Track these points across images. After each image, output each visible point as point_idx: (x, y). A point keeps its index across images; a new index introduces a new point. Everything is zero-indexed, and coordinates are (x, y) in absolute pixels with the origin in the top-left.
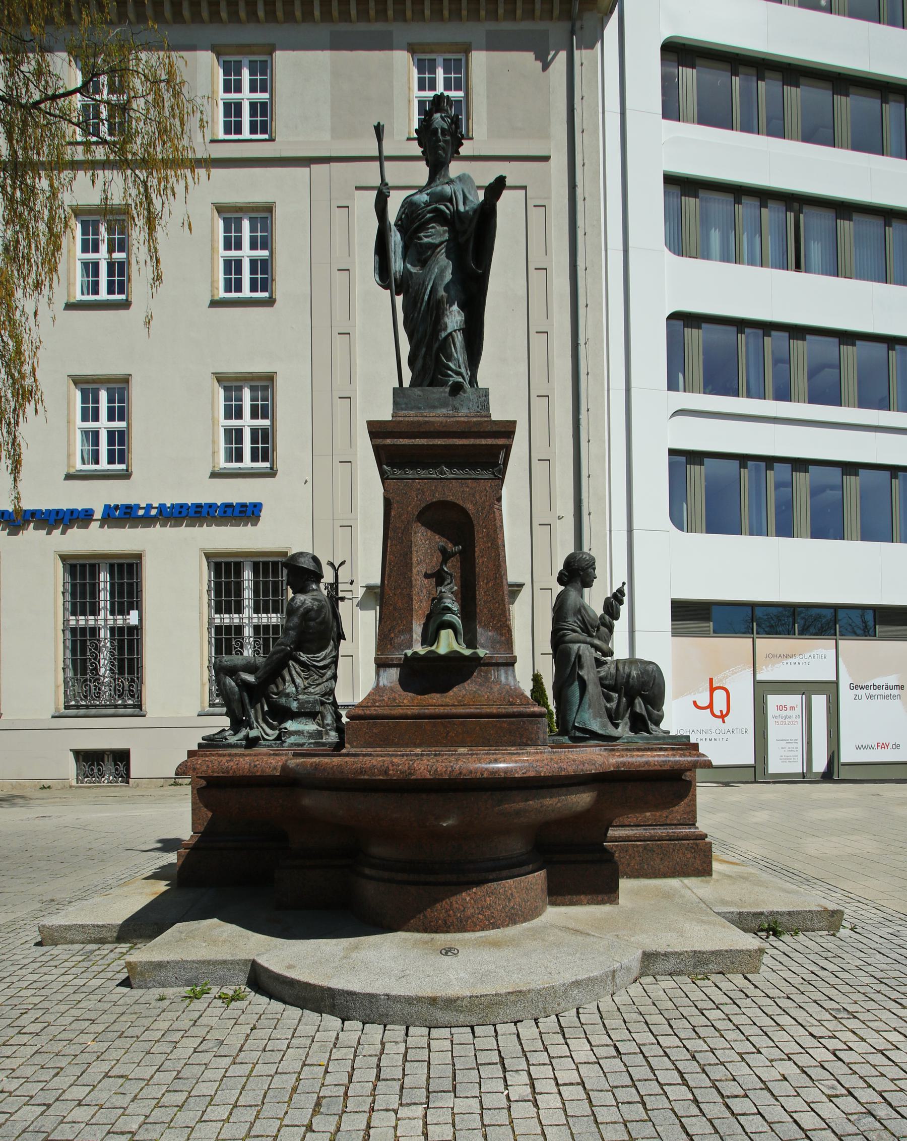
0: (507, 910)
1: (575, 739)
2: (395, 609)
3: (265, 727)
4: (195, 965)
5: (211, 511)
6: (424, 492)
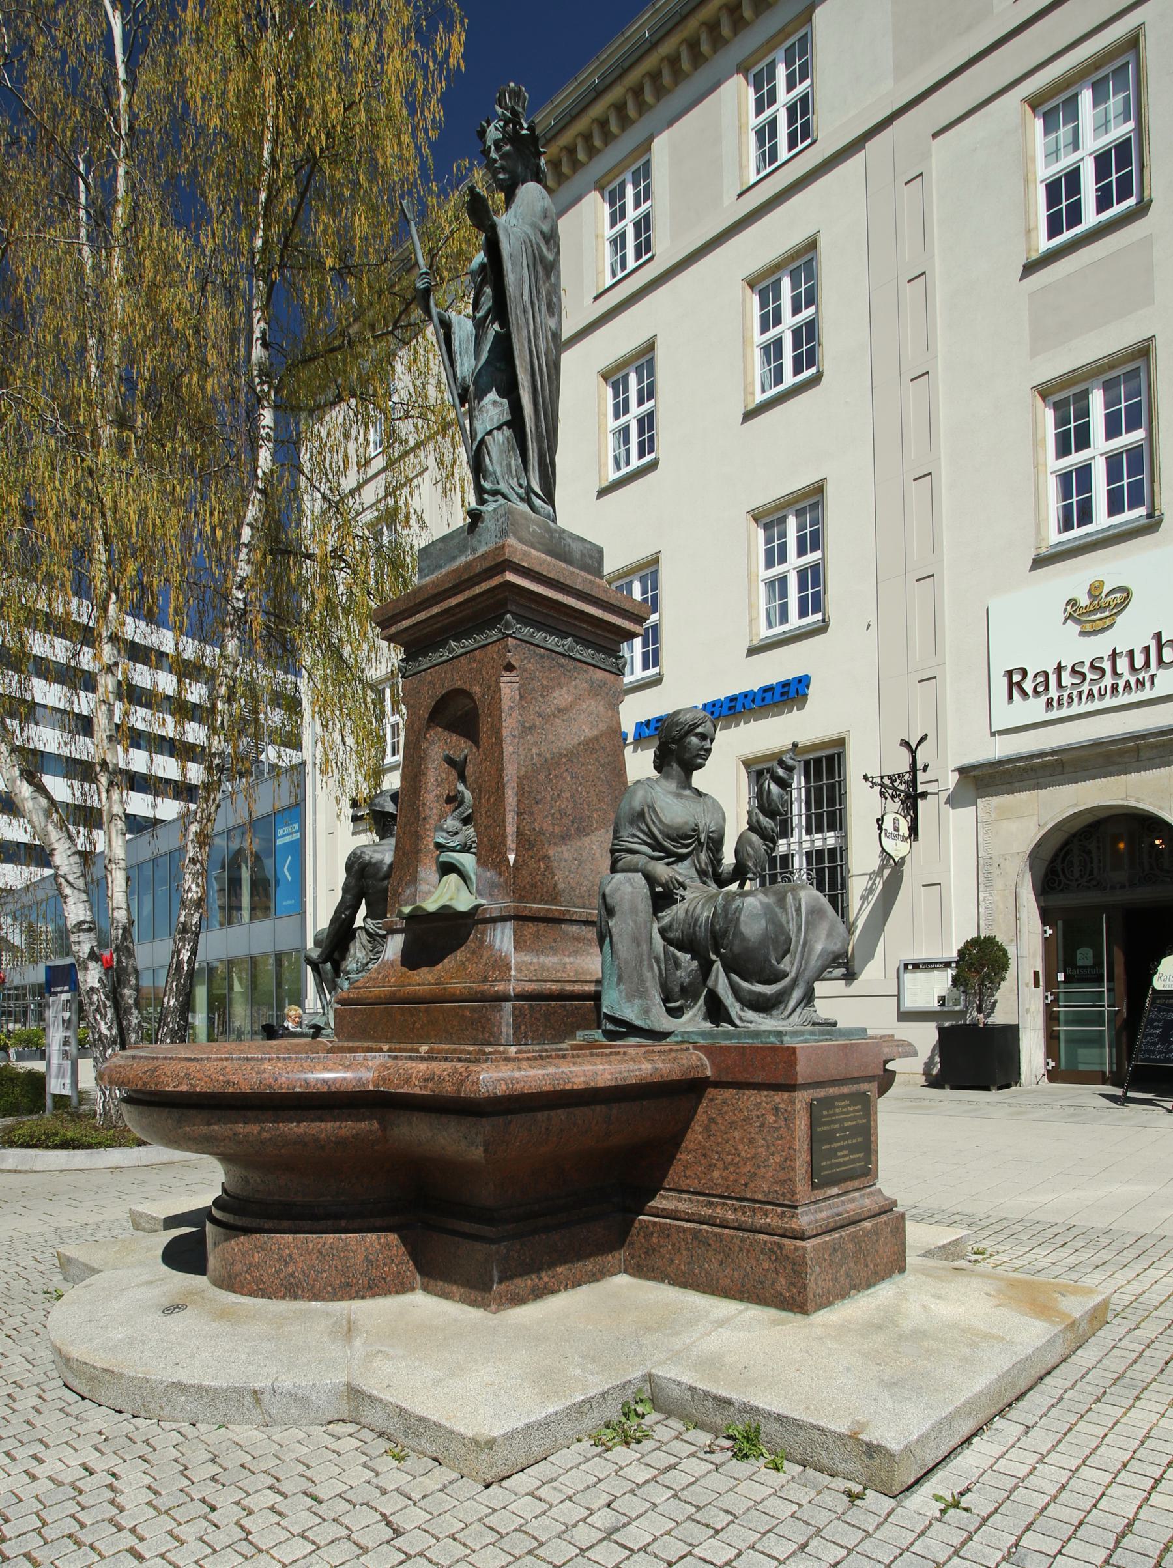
0: (282, 1276)
1: (611, 1035)
5: (748, 702)
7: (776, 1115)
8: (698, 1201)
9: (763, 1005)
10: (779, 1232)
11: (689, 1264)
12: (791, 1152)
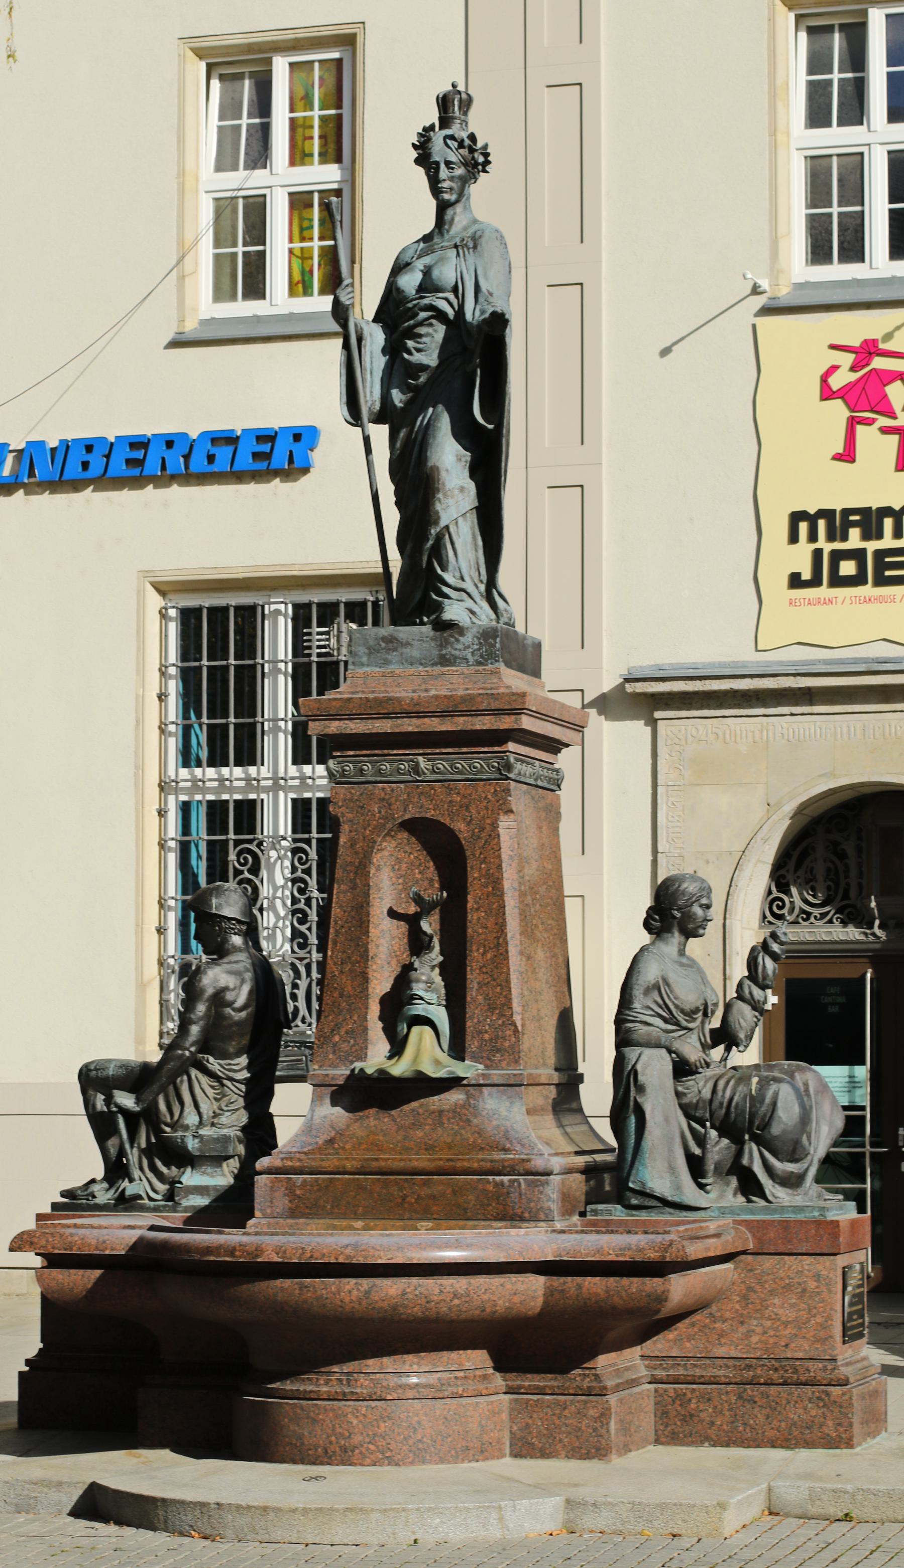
0: (411, 1442)
2: (341, 995)
4: (27, 1486)
6: (390, 805)
7: (818, 1281)
8: (735, 1366)
9: (792, 1182)
10: (825, 1382)
11: (733, 1422)
12: (832, 1312)
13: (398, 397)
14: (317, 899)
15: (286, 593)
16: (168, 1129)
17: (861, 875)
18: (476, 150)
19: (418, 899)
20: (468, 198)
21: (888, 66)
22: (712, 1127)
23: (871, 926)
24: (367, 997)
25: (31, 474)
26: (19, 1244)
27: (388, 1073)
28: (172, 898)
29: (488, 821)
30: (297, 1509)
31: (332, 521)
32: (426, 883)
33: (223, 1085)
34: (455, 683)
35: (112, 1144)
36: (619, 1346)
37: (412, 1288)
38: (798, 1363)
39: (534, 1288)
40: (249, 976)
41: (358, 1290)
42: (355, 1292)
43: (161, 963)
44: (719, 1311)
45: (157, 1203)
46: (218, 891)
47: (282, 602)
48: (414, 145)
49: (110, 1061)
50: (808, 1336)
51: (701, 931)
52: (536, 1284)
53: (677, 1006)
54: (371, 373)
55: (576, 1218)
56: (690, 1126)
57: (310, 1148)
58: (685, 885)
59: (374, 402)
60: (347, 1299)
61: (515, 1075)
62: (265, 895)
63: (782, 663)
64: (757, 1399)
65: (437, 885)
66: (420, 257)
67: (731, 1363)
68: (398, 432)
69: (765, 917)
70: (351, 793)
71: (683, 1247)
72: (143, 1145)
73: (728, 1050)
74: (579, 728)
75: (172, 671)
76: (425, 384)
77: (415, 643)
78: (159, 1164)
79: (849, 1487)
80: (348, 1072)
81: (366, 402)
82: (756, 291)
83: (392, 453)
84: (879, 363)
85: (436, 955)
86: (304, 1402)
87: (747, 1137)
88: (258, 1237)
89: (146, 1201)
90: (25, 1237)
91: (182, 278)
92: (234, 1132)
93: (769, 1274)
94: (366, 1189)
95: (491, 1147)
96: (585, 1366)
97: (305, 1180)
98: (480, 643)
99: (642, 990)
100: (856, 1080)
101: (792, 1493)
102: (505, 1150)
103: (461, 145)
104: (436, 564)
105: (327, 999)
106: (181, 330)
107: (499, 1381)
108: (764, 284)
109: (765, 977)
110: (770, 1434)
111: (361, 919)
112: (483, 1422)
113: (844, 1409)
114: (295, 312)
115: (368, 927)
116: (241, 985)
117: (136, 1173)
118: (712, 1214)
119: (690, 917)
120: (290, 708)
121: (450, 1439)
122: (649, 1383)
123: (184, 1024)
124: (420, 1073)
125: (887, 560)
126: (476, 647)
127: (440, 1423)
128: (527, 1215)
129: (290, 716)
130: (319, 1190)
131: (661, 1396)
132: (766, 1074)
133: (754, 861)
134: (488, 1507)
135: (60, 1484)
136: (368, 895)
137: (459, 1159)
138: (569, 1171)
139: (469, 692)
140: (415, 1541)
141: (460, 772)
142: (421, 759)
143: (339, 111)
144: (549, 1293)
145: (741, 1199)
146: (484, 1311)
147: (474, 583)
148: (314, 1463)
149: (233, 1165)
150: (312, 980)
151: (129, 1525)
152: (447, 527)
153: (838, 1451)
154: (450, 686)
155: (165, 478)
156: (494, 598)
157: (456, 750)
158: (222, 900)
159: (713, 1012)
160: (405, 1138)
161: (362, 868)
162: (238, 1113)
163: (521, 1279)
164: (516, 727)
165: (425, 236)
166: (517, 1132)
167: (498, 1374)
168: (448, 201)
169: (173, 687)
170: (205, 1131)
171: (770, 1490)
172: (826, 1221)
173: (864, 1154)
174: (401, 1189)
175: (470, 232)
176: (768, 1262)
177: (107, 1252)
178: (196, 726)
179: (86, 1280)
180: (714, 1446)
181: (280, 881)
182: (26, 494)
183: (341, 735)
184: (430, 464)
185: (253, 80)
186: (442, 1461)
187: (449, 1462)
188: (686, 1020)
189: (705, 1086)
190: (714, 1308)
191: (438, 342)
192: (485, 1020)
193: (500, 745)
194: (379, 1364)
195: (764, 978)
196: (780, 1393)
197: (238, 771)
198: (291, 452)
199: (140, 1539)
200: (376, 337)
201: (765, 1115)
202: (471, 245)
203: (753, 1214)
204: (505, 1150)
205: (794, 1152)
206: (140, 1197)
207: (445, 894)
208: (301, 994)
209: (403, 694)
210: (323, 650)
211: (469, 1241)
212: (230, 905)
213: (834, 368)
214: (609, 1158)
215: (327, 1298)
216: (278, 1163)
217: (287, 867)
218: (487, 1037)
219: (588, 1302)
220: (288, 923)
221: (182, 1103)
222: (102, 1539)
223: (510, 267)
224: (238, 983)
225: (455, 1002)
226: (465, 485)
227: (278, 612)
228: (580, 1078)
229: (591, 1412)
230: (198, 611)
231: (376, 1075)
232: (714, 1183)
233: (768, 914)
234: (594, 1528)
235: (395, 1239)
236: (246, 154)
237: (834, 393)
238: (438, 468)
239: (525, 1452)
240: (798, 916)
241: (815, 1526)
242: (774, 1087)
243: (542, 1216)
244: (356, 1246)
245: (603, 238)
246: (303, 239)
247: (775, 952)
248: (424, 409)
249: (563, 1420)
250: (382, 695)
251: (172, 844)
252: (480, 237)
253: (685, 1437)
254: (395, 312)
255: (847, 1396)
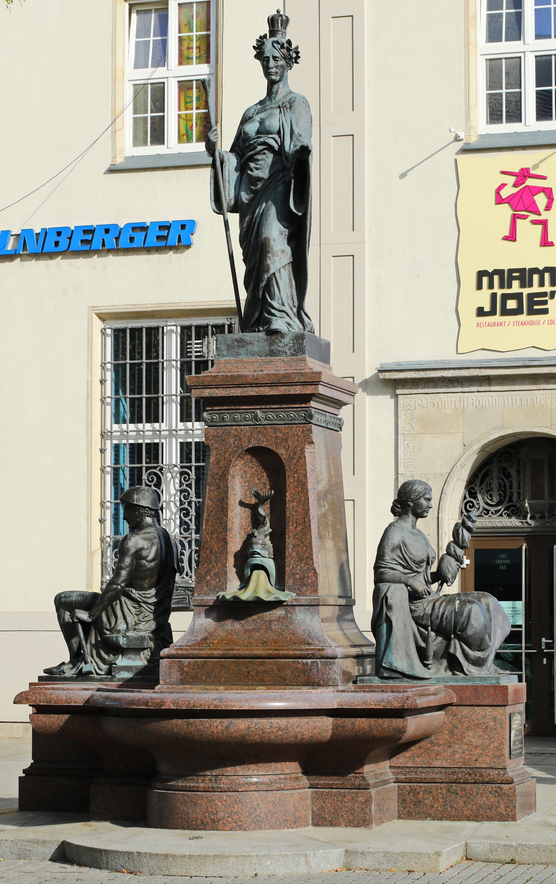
0: (253, 817)
2: (211, 552)
3: (100, 663)
4: (24, 843)
6: (240, 439)
7: (495, 721)
8: (446, 772)
9: (479, 663)
10: (499, 782)
11: (444, 806)
12: (503, 740)
13: (245, 197)
14: (195, 502)
15: (177, 319)
16: (108, 632)
17: (519, 488)
18: (292, 50)
19: (257, 495)
20: (287, 79)
21: (535, 5)
22: (432, 630)
23: (525, 517)
24: (227, 553)
25: (25, 247)
26: (19, 699)
27: (239, 598)
28: (109, 502)
29: (299, 449)
30: (185, 855)
31: (206, 275)
32: (262, 485)
33: (141, 606)
34: (279, 366)
35: (75, 641)
36: (377, 760)
37: (254, 724)
38: (483, 771)
39: (326, 725)
40: (156, 541)
41: (222, 725)
42: (220, 727)
43: (102, 540)
44: (436, 739)
45: (101, 676)
46: (138, 491)
47: (174, 325)
48: (254, 47)
49: (73, 592)
50: (489, 754)
51: (425, 514)
52: (327, 723)
53: (411, 559)
54: (229, 182)
55: (351, 684)
56: (419, 630)
57: (193, 643)
58: (415, 487)
59: (230, 200)
60: (215, 731)
61: (314, 599)
62: (164, 499)
63: (472, 361)
64: (458, 792)
65: (268, 487)
66: (258, 113)
67: (443, 770)
68: (245, 217)
69: (462, 512)
70: (217, 432)
71: (415, 700)
72: (93, 642)
73: (441, 585)
74: (352, 394)
75: (109, 366)
76: (261, 189)
77: (255, 343)
78: (103, 653)
79: (513, 843)
80: (215, 598)
81: (226, 200)
82: (457, 139)
83: (241, 231)
84: (530, 182)
85: (267, 528)
86: (190, 793)
87: (453, 636)
88: (162, 694)
89: (95, 675)
90: (23, 695)
91: (114, 132)
92: (147, 634)
93: (466, 718)
94: (226, 667)
95: (301, 642)
96: (356, 771)
97: (189, 662)
98: (294, 343)
99: (390, 549)
100: (517, 609)
101: (479, 847)
102: (309, 644)
103: (282, 46)
104: (267, 296)
105: (203, 554)
106: (114, 163)
107: (305, 781)
108: (462, 135)
109: (463, 541)
110: (466, 813)
111: (223, 507)
112: (296, 805)
113: (511, 797)
114: (182, 152)
115: (227, 511)
116: (152, 547)
117: (89, 659)
118: (432, 682)
119: (419, 505)
120: (179, 388)
121: (276, 815)
122: (394, 782)
123: (117, 572)
124: (258, 598)
125: (535, 299)
126: (291, 345)
127: (271, 805)
128: (322, 682)
129: (179, 393)
130: (198, 668)
131: (402, 790)
132: (464, 599)
133: (455, 479)
134: (299, 854)
135: (44, 842)
136: (227, 492)
137: (281, 649)
138: (347, 657)
139: (287, 372)
140: (256, 875)
141: (282, 419)
142: (258, 411)
143: (208, 33)
144: (335, 727)
145: (449, 673)
146: (297, 738)
147: (290, 307)
148: (196, 829)
149: (147, 653)
150: (192, 550)
151: (85, 866)
152: (274, 274)
153: (507, 823)
154: (276, 368)
155: (105, 250)
156: (303, 319)
157: (280, 406)
158: (140, 496)
159: (432, 562)
160: (249, 637)
161: (223, 477)
162: (149, 623)
163: (319, 719)
164: (315, 392)
165: (260, 101)
166: (316, 633)
167: (304, 777)
168: (275, 80)
169: (109, 376)
170: (130, 634)
171: (466, 845)
172: (500, 686)
173: (521, 654)
174: (247, 667)
175: (288, 98)
176: (465, 711)
177: (72, 704)
178: (123, 399)
179: (59, 721)
180: (433, 820)
181: (173, 492)
182: (21, 261)
183: (211, 397)
184: (264, 236)
185: (157, 14)
186: (271, 828)
187: (276, 829)
188: (416, 567)
189: (427, 606)
190: (433, 738)
191: (268, 164)
192: (297, 567)
193: (306, 403)
194: (234, 770)
195: (463, 542)
196: (472, 788)
197: (148, 426)
198: (179, 236)
199: (92, 874)
200: (232, 161)
201: (463, 623)
202: (288, 106)
203: (456, 682)
204: (309, 644)
205: (481, 646)
206: (91, 673)
207: (273, 492)
208: (185, 558)
209: (248, 373)
210: (199, 354)
211: (287, 696)
212: (145, 499)
213: (503, 185)
214: (372, 650)
215: (203, 731)
216: (174, 652)
217: (177, 483)
218: (298, 576)
219: (358, 733)
220: (178, 516)
221: (116, 617)
222: (69, 874)
223: (311, 120)
224: (150, 546)
225: (279, 555)
226: (285, 249)
227: (172, 331)
228: (353, 602)
229: (360, 799)
230: (124, 330)
231: (232, 599)
232: (433, 663)
233: (464, 511)
234: (362, 867)
235: (244, 695)
236: (153, 58)
237: (503, 200)
238: (269, 239)
239: (320, 823)
240: (482, 512)
241: (491, 868)
242: (469, 606)
243: (331, 683)
244: (220, 700)
245: (366, 133)
246: (187, 109)
247: (469, 527)
248: (259, 204)
249: (343, 804)
250: (235, 374)
251: (109, 469)
252: (294, 101)
253: (416, 814)
254: (243, 146)
255: (512, 790)
